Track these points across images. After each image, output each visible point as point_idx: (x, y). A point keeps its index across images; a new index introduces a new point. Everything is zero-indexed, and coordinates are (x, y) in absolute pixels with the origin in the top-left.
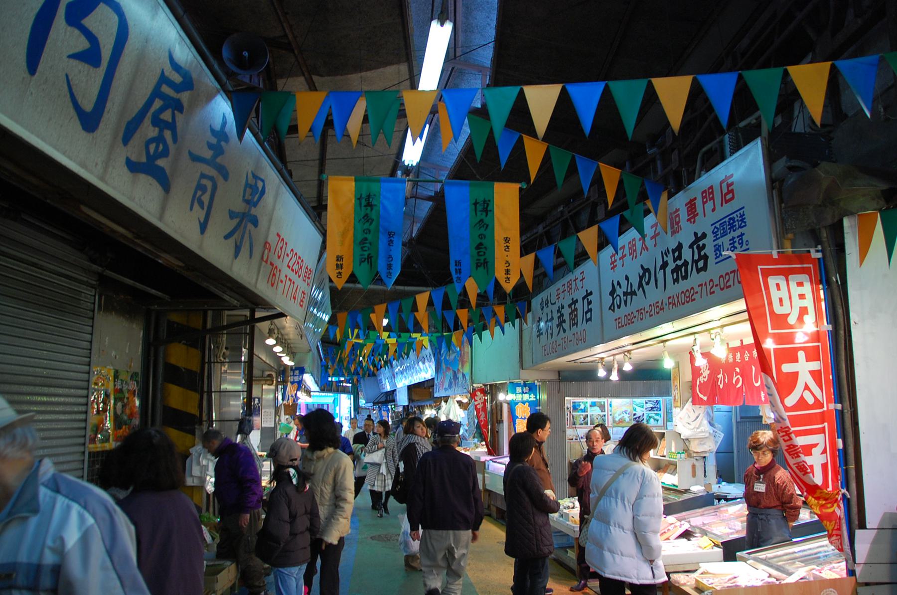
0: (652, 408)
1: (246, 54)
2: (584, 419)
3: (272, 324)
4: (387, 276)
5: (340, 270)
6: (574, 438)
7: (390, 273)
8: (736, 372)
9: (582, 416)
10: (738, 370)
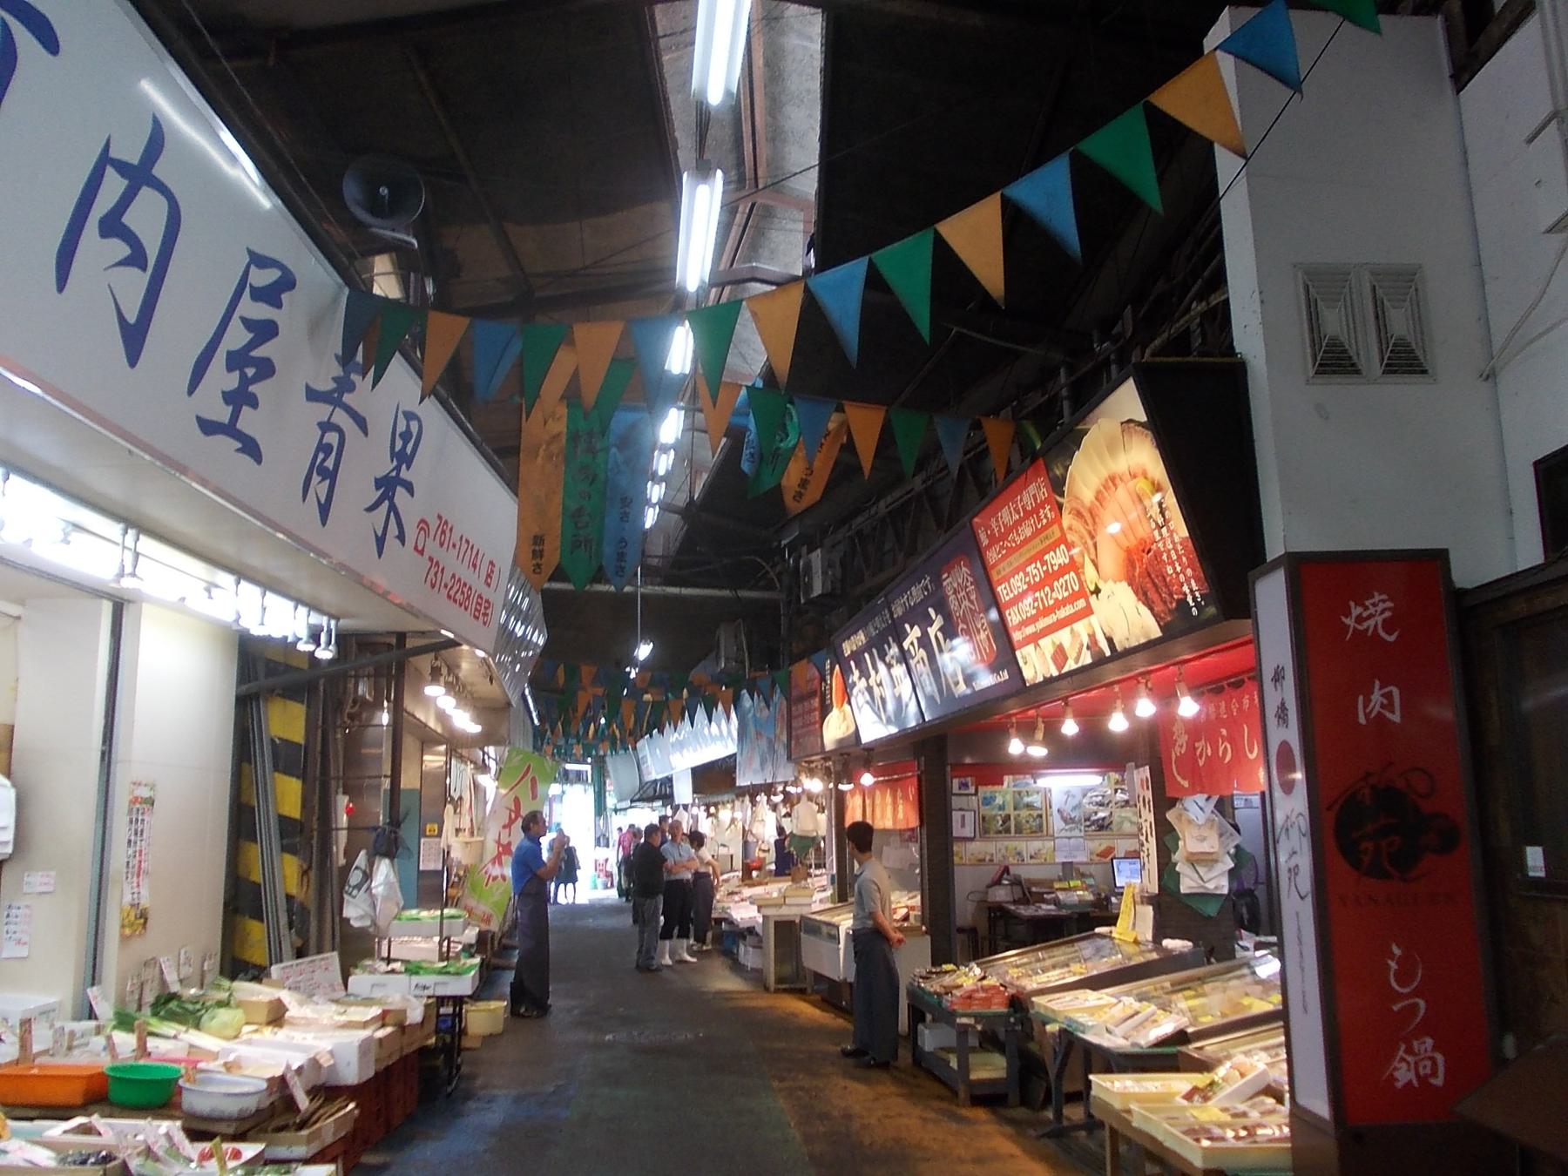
0: (1127, 802)
1: (384, 191)
2: (1004, 822)
3: (436, 659)
4: (617, 573)
5: (538, 561)
6: (988, 858)
7: (622, 569)
8: (1222, 737)
9: (999, 818)
10: (1224, 732)
